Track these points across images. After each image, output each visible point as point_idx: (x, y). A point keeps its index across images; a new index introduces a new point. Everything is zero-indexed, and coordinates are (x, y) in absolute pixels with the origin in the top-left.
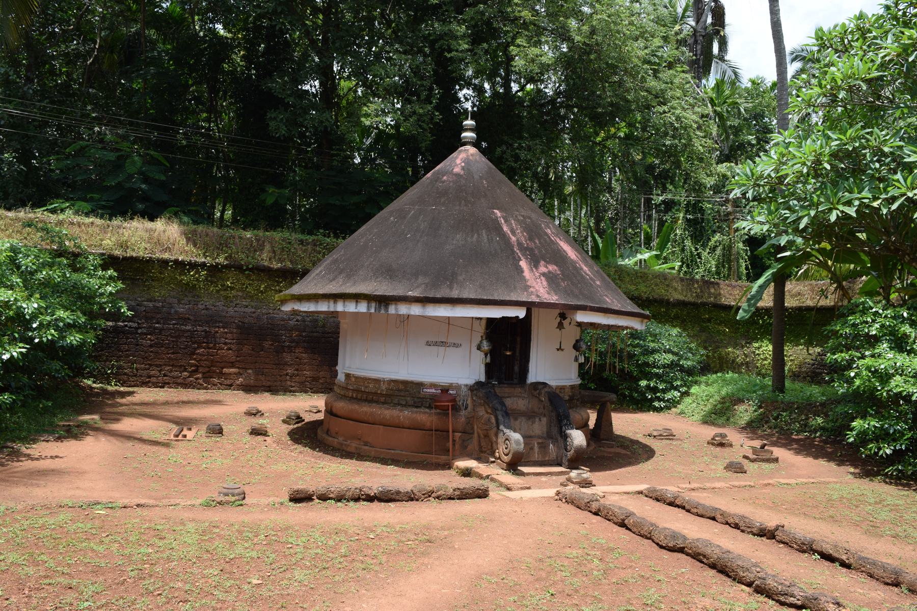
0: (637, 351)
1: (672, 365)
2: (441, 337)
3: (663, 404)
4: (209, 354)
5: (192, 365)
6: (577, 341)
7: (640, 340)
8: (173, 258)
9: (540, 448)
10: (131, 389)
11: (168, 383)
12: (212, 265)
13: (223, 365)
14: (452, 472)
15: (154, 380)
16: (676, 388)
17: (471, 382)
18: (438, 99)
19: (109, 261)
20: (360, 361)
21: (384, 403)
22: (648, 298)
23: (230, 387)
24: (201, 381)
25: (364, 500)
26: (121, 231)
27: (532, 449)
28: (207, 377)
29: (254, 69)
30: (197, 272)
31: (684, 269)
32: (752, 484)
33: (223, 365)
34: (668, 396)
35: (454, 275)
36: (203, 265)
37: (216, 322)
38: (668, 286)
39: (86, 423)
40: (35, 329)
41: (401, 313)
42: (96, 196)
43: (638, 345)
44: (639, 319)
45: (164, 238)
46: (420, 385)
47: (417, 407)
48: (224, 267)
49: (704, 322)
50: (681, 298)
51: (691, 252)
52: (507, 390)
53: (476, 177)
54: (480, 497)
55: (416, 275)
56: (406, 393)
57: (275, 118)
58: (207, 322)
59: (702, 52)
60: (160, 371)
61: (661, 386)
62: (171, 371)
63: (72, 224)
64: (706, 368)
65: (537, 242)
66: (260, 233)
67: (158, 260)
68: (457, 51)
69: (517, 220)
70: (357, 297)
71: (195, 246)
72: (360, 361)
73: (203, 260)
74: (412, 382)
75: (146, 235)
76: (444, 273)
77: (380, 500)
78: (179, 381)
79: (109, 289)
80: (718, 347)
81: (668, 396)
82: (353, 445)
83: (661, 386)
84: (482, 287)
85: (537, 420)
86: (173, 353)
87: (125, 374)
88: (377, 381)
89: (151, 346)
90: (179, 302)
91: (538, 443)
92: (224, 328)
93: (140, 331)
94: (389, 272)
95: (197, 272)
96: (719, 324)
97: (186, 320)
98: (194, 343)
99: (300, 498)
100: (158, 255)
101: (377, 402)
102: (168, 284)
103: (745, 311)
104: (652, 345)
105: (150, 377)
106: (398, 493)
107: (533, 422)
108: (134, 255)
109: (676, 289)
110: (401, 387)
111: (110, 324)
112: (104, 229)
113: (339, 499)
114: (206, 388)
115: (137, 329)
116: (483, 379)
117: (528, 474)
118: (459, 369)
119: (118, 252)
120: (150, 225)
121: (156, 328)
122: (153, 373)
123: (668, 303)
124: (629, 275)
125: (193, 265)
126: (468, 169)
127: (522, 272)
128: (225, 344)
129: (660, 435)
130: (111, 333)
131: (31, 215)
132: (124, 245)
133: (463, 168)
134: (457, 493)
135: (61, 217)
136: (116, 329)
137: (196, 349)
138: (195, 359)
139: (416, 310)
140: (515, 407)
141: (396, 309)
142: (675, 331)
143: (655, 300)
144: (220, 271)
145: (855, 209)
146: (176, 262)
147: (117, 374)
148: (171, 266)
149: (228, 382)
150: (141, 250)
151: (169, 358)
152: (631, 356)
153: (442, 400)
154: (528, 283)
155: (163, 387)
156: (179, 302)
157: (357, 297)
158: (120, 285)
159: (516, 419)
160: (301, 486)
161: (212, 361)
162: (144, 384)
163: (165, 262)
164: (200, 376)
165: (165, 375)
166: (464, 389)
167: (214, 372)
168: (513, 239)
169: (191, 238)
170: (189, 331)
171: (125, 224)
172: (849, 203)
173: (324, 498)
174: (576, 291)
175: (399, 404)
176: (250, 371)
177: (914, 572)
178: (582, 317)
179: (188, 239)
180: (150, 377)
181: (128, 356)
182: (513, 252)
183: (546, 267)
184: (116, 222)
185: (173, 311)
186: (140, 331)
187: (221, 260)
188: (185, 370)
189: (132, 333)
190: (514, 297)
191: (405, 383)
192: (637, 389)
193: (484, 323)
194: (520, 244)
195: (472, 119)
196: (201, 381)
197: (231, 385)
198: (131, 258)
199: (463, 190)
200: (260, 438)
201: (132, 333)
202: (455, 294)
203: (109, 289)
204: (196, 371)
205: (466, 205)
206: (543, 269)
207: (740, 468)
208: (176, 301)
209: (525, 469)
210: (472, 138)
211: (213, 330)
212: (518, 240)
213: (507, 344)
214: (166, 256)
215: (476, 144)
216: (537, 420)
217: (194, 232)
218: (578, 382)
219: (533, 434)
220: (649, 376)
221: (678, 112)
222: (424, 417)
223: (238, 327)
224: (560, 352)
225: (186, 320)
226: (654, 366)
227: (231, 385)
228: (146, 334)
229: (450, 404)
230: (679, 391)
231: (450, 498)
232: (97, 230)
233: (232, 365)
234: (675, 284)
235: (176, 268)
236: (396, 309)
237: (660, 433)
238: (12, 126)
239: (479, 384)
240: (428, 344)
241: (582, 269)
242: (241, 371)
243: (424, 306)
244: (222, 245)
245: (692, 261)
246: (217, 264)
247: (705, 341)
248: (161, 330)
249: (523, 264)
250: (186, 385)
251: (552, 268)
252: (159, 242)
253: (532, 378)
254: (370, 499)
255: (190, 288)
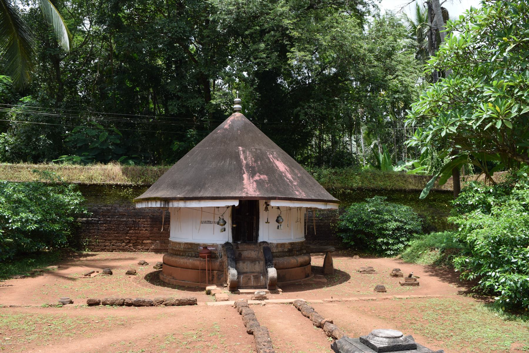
0: (376, 221)
1: (398, 229)
2: (204, 217)
3: (392, 252)
4: (135, 233)
5: (127, 239)
6: (278, 217)
7: (379, 214)
8: (115, 183)
9: (254, 278)
10: (95, 253)
11: (115, 249)
12: (135, 186)
13: (143, 238)
14: (204, 292)
15: (107, 248)
16: (402, 242)
17: (223, 242)
18: (258, 85)
19: (82, 188)
20: (182, 234)
21: (182, 256)
22: (391, 190)
23: (147, 250)
24: (132, 248)
25: (126, 305)
26: (90, 171)
27: (250, 279)
28: (135, 245)
29: (170, 79)
30: (128, 190)
31: (434, 170)
32: (374, 298)
33: (143, 238)
34: (395, 247)
35: (205, 184)
36: (131, 186)
37: (139, 216)
38: (405, 181)
39: (48, 270)
40: (11, 223)
41: (175, 206)
42: (87, 153)
43: (378, 218)
44: (324, 203)
45: (111, 172)
46: (198, 245)
47: (197, 257)
48: (143, 186)
49: (431, 201)
50: (414, 188)
51: (437, 160)
52: (246, 246)
53: (235, 129)
54: (191, 305)
55: (185, 186)
56: (191, 250)
57: (171, 105)
58: (134, 216)
59: (436, 39)
60: (111, 243)
61: (391, 241)
62: (116, 243)
63: (66, 169)
64: (427, 229)
65: (259, 163)
66: (162, 167)
67: (107, 185)
68: (260, 58)
69: (251, 152)
70: (155, 199)
71: (127, 176)
72: (182, 234)
73: (131, 183)
74: (194, 244)
75: (102, 172)
76: (201, 186)
77: (135, 306)
78: (121, 248)
79: (76, 201)
80: (442, 216)
81: (395, 247)
82: (167, 279)
83: (391, 241)
84: (217, 190)
85: (257, 263)
86: (117, 233)
87: (93, 245)
88: (179, 244)
89: (105, 230)
90: (120, 206)
91: (253, 276)
92: (143, 219)
93: (99, 222)
94: (174, 185)
95: (128, 190)
96: (442, 202)
97: (123, 215)
98: (127, 228)
99: (92, 304)
100: (108, 182)
101: (180, 255)
102: (114, 197)
103: (424, 193)
104: (386, 217)
105: (105, 246)
106: (144, 302)
107: (255, 264)
108: (95, 183)
109: (410, 183)
110: (190, 246)
111: (289, 176)
112: (81, 171)
113: (112, 304)
114: (135, 251)
115: (98, 221)
116: (231, 241)
117: (242, 293)
118: (217, 236)
119: (87, 182)
120: (104, 167)
121: (108, 221)
122: (107, 244)
123: (405, 191)
124: (379, 176)
125: (125, 187)
126: (232, 125)
127: (243, 180)
128: (144, 227)
129: (364, 271)
130: (85, 224)
131: (46, 166)
132: (91, 178)
133: (229, 125)
134: (177, 302)
135: (61, 165)
136: (87, 221)
137: (128, 231)
138: (128, 236)
139: (181, 204)
140: (250, 256)
141: (173, 205)
142: (404, 208)
143: (397, 190)
144: (139, 188)
145: (456, 127)
146: (117, 185)
147: (89, 245)
148: (114, 188)
149: (146, 248)
150: (98, 180)
151: (115, 236)
152: (373, 224)
153: (209, 253)
154: (244, 187)
155: (112, 251)
156: (120, 206)
157: (155, 199)
158: (83, 199)
159: (244, 263)
160: (91, 297)
161: (137, 236)
162: (103, 250)
163: (110, 186)
164: (131, 245)
165: (113, 245)
166: (220, 247)
167: (139, 242)
168: (245, 162)
169: (125, 172)
170: (125, 221)
171: (93, 167)
172: (453, 124)
173: (105, 304)
174: (274, 189)
175: (189, 256)
176: (158, 242)
177: (2, 309)
178: (273, 204)
179: (123, 173)
180: (105, 246)
181: (94, 236)
182: (241, 169)
183: (259, 177)
184: (89, 166)
185: (116, 211)
186: (99, 222)
187: (140, 183)
188: (124, 242)
189: (96, 224)
190: (232, 194)
191: (191, 244)
192: (376, 244)
193: (230, 209)
194: (247, 165)
195: (239, 97)
196: (132, 248)
197: (148, 249)
198: (94, 184)
199: (231, 137)
200: (132, 277)
201: (96, 224)
202: (200, 195)
203: (76, 201)
204: (129, 242)
205: (224, 146)
206: (257, 178)
207: (382, 289)
208: (118, 206)
209: (241, 291)
210: (240, 108)
211: (137, 220)
212: (247, 163)
213: (245, 217)
214: (111, 182)
215: (242, 111)
216: (257, 263)
217: (126, 169)
218: (303, 240)
219: (255, 271)
220: (384, 236)
221: (400, 77)
222: (197, 262)
223: (151, 218)
224: (267, 224)
225: (123, 215)
226: (387, 229)
227: (148, 249)
228: (103, 224)
229: (206, 255)
230: (404, 244)
231: (173, 305)
232: (77, 171)
233: (148, 238)
234: (410, 180)
235: (117, 188)
236: (173, 205)
237: (364, 269)
238: (47, 122)
239: (227, 244)
240: (202, 223)
241: (286, 176)
242: (153, 242)
243: (185, 202)
244: (142, 174)
245: (438, 165)
246: (138, 185)
247: (433, 213)
248: (110, 221)
249: (245, 176)
250: (124, 250)
251: (264, 177)
252: (108, 176)
253: (261, 239)
254: (129, 305)
255: (125, 198)
